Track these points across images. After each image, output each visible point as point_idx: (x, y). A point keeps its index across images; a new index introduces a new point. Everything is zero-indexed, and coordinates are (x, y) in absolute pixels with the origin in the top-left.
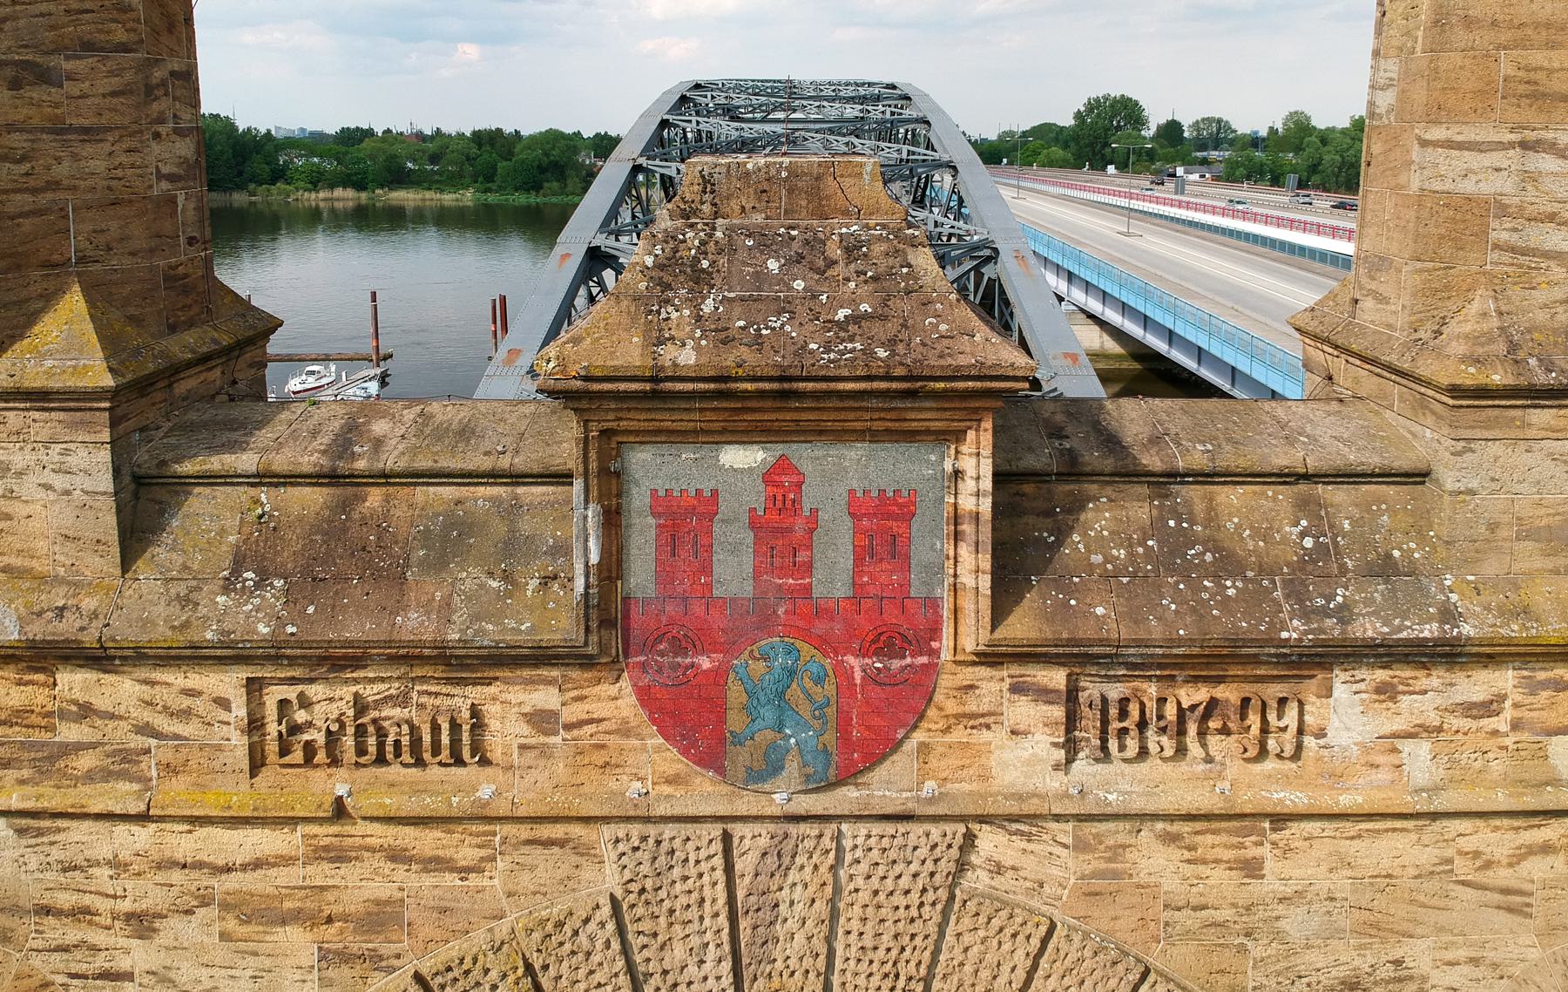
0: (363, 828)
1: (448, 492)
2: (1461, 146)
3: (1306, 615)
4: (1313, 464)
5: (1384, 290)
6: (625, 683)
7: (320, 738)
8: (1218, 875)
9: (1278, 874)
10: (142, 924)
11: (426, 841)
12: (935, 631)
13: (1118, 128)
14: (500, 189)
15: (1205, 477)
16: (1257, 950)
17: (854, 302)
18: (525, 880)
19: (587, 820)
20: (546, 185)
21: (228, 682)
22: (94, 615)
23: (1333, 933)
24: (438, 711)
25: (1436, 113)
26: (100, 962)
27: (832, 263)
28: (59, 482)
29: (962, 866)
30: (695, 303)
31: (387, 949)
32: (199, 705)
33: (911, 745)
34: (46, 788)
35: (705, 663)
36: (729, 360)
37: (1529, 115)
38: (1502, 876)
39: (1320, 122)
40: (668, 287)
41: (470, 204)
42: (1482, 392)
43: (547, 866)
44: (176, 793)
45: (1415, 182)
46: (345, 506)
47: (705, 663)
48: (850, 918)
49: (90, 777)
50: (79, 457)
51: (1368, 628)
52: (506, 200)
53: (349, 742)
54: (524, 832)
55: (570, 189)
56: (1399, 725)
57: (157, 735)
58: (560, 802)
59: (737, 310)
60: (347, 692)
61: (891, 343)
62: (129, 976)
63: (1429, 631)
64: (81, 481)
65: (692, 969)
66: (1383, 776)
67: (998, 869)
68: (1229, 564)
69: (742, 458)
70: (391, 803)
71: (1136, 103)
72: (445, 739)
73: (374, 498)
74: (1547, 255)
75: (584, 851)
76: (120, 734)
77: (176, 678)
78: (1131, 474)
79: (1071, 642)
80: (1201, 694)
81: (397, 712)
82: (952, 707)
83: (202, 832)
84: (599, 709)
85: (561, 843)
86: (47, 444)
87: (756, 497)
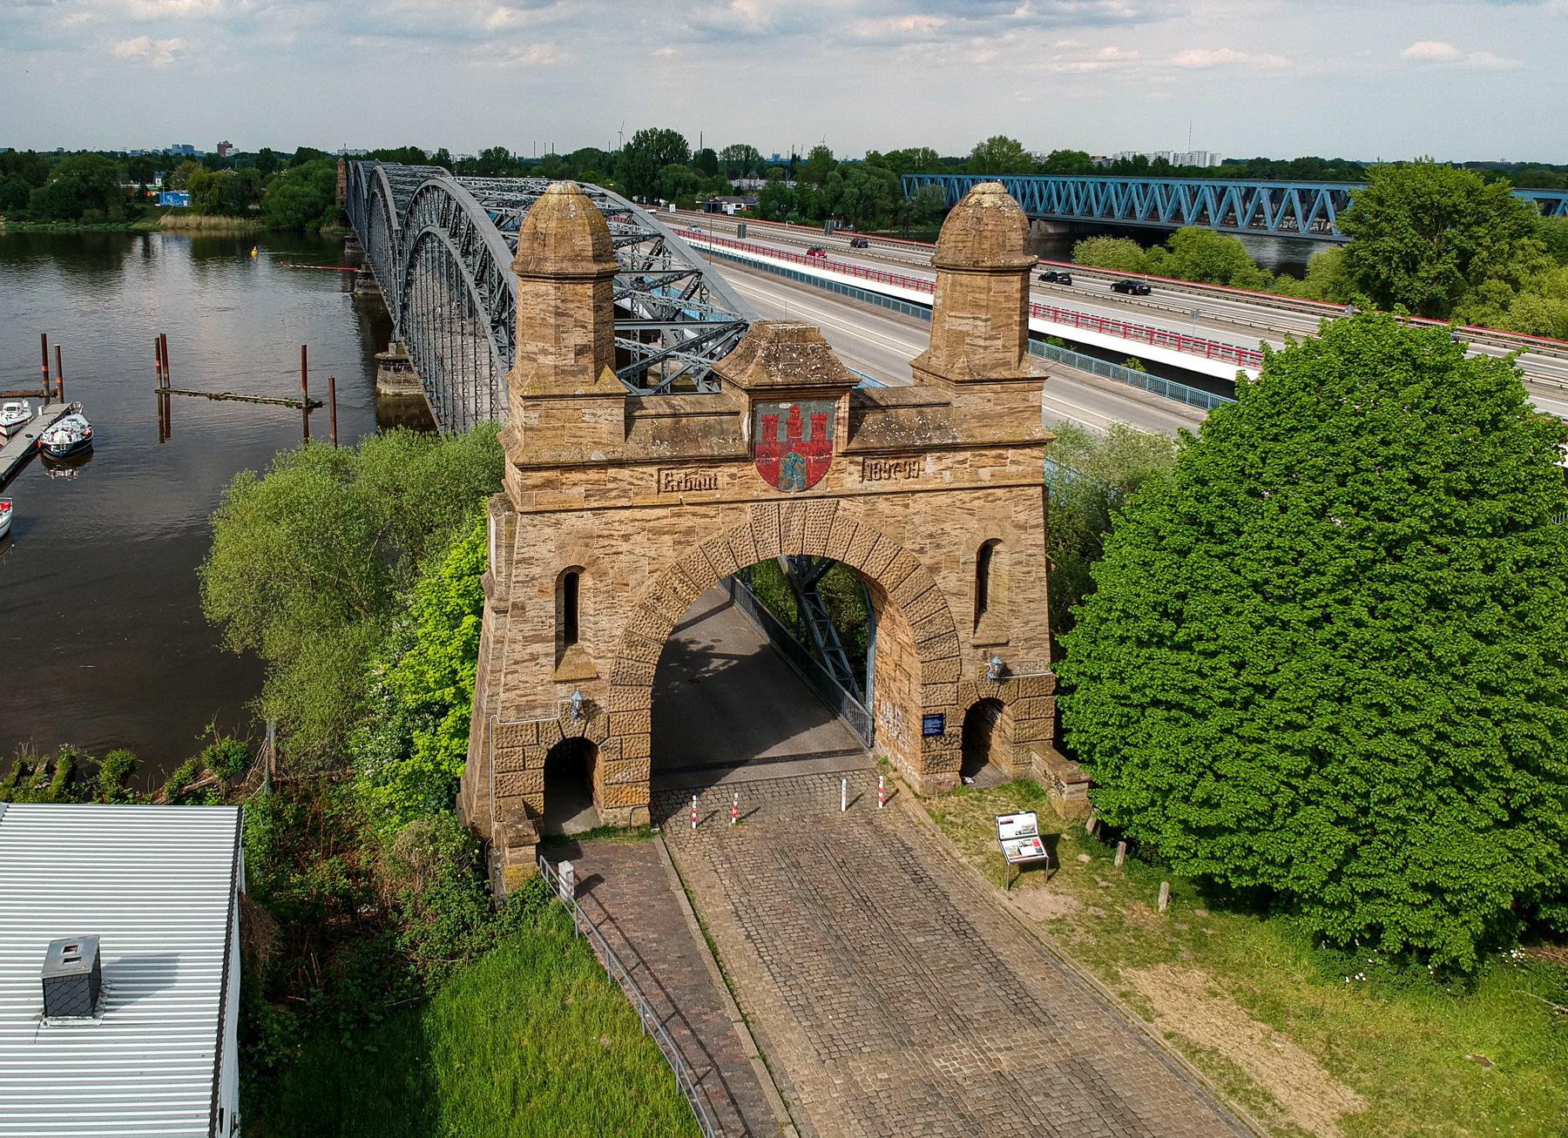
6: (754, 466)
9: (914, 507)
10: (626, 538)
11: (701, 510)
13: (665, 162)
14: (34, 217)
15: (895, 407)
20: (86, 212)
21: (653, 470)
23: (926, 522)
26: (614, 550)
29: (836, 509)
36: (791, 379)
37: (975, 310)
38: (968, 505)
39: (838, 156)
43: (733, 515)
44: (638, 501)
46: (677, 423)
49: (615, 498)
50: (616, 411)
51: (936, 441)
52: (44, 229)
54: (727, 506)
68: (902, 428)
69: (784, 406)
70: (690, 500)
71: (680, 137)
73: (684, 420)
75: (741, 510)
78: (878, 407)
84: (746, 473)
87: (788, 416)
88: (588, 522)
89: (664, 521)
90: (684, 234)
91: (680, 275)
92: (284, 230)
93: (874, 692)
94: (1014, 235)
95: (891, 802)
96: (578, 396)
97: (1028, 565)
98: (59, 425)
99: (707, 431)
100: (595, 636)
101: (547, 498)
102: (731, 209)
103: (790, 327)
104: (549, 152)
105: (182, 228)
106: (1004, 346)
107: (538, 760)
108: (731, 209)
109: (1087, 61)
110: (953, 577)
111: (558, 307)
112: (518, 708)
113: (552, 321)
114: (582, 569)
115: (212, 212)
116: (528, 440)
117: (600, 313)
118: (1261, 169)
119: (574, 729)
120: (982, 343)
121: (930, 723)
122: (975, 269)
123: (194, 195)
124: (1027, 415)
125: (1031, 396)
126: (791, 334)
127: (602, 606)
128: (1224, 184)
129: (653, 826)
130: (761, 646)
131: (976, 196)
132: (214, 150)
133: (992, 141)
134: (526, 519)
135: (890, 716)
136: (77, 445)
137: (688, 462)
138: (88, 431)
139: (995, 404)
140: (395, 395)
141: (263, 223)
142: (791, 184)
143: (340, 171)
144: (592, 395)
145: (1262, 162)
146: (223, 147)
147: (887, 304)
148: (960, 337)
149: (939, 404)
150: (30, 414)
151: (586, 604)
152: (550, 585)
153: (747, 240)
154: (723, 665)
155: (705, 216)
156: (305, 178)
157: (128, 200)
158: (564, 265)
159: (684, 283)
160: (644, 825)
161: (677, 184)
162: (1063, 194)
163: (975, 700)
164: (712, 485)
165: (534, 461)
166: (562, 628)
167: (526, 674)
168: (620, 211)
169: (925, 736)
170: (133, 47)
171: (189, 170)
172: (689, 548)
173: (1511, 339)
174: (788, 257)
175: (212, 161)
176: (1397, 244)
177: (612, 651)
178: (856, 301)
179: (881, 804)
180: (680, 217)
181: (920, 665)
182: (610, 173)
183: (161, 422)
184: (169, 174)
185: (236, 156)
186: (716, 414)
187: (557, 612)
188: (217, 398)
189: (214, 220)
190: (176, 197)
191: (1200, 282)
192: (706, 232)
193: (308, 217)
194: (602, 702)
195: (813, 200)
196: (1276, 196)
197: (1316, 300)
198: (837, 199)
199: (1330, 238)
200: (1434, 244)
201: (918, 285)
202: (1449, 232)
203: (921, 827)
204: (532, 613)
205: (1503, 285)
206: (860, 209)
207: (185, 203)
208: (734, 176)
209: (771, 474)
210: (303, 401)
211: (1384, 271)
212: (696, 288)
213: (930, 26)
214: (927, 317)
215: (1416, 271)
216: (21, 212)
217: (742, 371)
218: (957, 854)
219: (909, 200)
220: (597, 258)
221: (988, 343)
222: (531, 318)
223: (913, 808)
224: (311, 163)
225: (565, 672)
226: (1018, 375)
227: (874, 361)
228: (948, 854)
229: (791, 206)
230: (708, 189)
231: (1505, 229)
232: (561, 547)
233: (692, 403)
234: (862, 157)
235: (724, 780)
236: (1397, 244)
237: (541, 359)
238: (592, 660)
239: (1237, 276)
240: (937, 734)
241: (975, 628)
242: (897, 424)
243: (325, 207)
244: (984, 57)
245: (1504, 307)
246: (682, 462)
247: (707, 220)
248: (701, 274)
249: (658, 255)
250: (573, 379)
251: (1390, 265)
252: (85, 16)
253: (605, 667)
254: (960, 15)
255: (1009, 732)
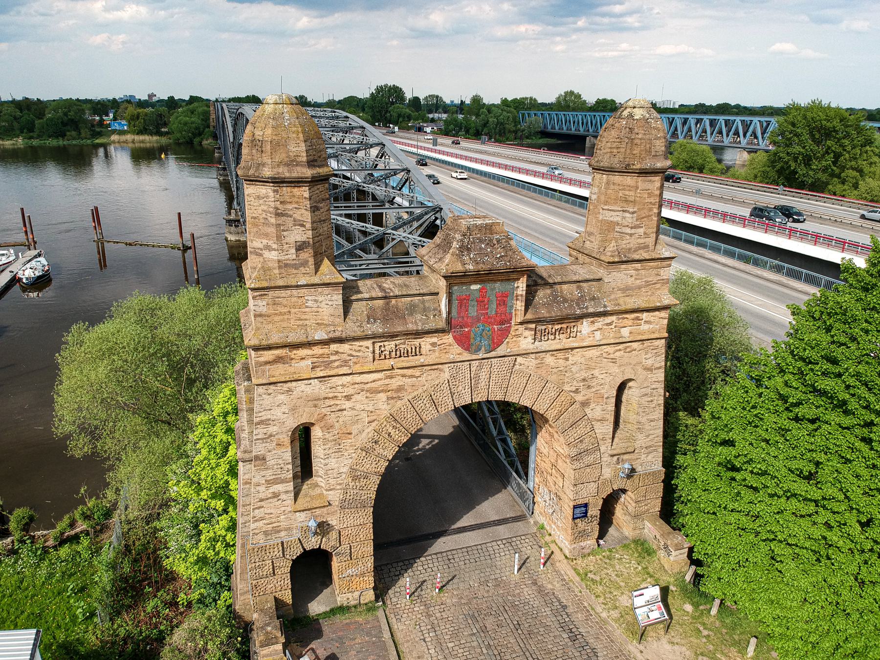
0: (396, 371)
1: (409, 299)
2: (610, 210)
3: (580, 309)
4: (580, 279)
5: (593, 240)
6: (451, 335)
7: (388, 353)
8: (561, 361)
10: (348, 398)
12: (511, 319)
13: (392, 103)
15: (560, 283)
16: (567, 375)
17: (500, 253)
18: (430, 378)
19: (442, 364)
20: (68, 133)
21: (369, 343)
22: (342, 331)
24: (411, 345)
25: (606, 203)
26: (338, 408)
27: (495, 245)
28: (330, 303)
29: (514, 364)
30: (469, 255)
31: (401, 395)
32: (362, 349)
33: (505, 342)
34: (327, 371)
35: (466, 330)
37: (625, 205)
38: (612, 356)
39: (487, 100)
40: (462, 252)
41: (22, 146)
42: (613, 263)
43: (434, 374)
44: (357, 368)
45: (601, 218)
46: (388, 304)
47: (466, 330)
48: (493, 377)
49: (337, 367)
50: (335, 297)
51: (591, 310)
53: (394, 353)
54: (429, 368)
55: (83, 135)
56: (594, 329)
57: (353, 356)
58: (438, 361)
59: (478, 256)
60: (394, 343)
61: (509, 261)
62: (345, 410)
63: (602, 310)
64: (335, 302)
65: (463, 391)
66: (591, 339)
67: (521, 365)
68: (565, 300)
69: (475, 287)
70: (400, 365)
72: (414, 350)
73: (393, 301)
74: (626, 234)
75: (441, 370)
76: (345, 357)
77: (357, 343)
78: (546, 284)
79: (539, 318)
80: (559, 326)
81: (403, 346)
82: (513, 334)
83: (362, 376)
85: (437, 369)
86: (327, 295)
88: (316, 388)
89: (380, 383)
90: (397, 142)
91: (395, 172)
92: (181, 144)
93: (534, 480)
94: (658, 142)
95: (548, 563)
96: (301, 286)
97: (651, 396)
98: (28, 266)
99: (412, 309)
100: (326, 474)
101: (279, 371)
102: (428, 130)
103: (479, 222)
104: (331, 98)
105: (124, 142)
106: (645, 233)
107: (285, 568)
108: (428, 130)
109: (612, 51)
110: (599, 408)
111: (277, 209)
112: (266, 533)
113: (273, 220)
114: (313, 424)
115: (140, 132)
116: (259, 325)
117: (316, 213)
118: (701, 109)
119: (312, 543)
120: (628, 231)
121: (578, 511)
122: (626, 170)
123: (130, 123)
124: (658, 286)
125: (662, 272)
126: (480, 228)
127: (331, 451)
128: (673, 116)
129: (377, 600)
130: (454, 427)
131: (628, 110)
132: (147, 98)
133: (566, 93)
134: (261, 390)
135: (547, 498)
136: (39, 277)
137: (397, 336)
138: (47, 268)
139: (636, 279)
140: (236, 241)
141: (170, 139)
142: (460, 116)
143: (211, 109)
144: (313, 285)
145: (702, 106)
146: (151, 96)
147: (518, 185)
148: (611, 226)
149: (594, 280)
150: (14, 257)
151: (318, 450)
152: (287, 440)
153: (438, 148)
154: (428, 444)
155: (414, 134)
156: (192, 113)
157: (93, 126)
158: (281, 170)
159: (399, 176)
160: (371, 602)
161: (399, 116)
162: (594, 122)
163: (610, 491)
164: (417, 352)
165: (264, 343)
166: (299, 469)
167: (270, 507)
168: (356, 128)
169: (574, 519)
170: (98, 39)
171: (126, 109)
172: (399, 402)
173: (871, 206)
174: (725, 217)
175: (141, 104)
176: (802, 150)
177: (340, 484)
178: (500, 184)
179: (542, 566)
180: (401, 134)
181: (572, 471)
182: (363, 110)
183: (100, 260)
184: (116, 111)
185: (158, 101)
186: (419, 295)
187: (293, 458)
188: (130, 244)
189: (142, 138)
190: (120, 124)
191: (687, 171)
192: (415, 143)
193: (195, 135)
194: (333, 521)
195: (473, 125)
196: (713, 123)
197: (751, 181)
198: (485, 124)
199: (739, 146)
200: (821, 150)
201: (581, 184)
202: (829, 143)
203: (571, 584)
204: (272, 462)
205: (855, 173)
206: (497, 131)
207: (126, 128)
208: (430, 112)
209: (464, 342)
210: (181, 246)
211: (793, 165)
212: (406, 180)
213: (533, 30)
214: (581, 206)
215: (810, 165)
216: (31, 134)
217: (440, 259)
218: (599, 609)
219: (523, 126)
220: (311, 163)
221: (633, 231)
222: (255, 218)
223: (564, 567)
224: (196, 104)
225: (302, 502)
226: (655, 255)
227: (516, 222)
228: (593, 609)
229: (461, 129)
230: (416, 119)
231: (859, 141)
232: (294, 409)
233: (400, 286)
234: (498, 102)
235: (431, 550)
236: (802, 150)
237: (267, 254)
238: (324, 492)
239: (707, 167)
240: (583, 517)
241: (612, 442)
242: (562, 297)
243: (204, 129)
244: (559, 48)
245: (856, 186)
246: (392, 336)
247: (415, 136)
248: (409, 171)
249: (381, 158)
250: (295, 271)
251: (797, 161)
252: (71, 22)
253: (335, 497)
254: (548, 24)
255: (631, 509)
